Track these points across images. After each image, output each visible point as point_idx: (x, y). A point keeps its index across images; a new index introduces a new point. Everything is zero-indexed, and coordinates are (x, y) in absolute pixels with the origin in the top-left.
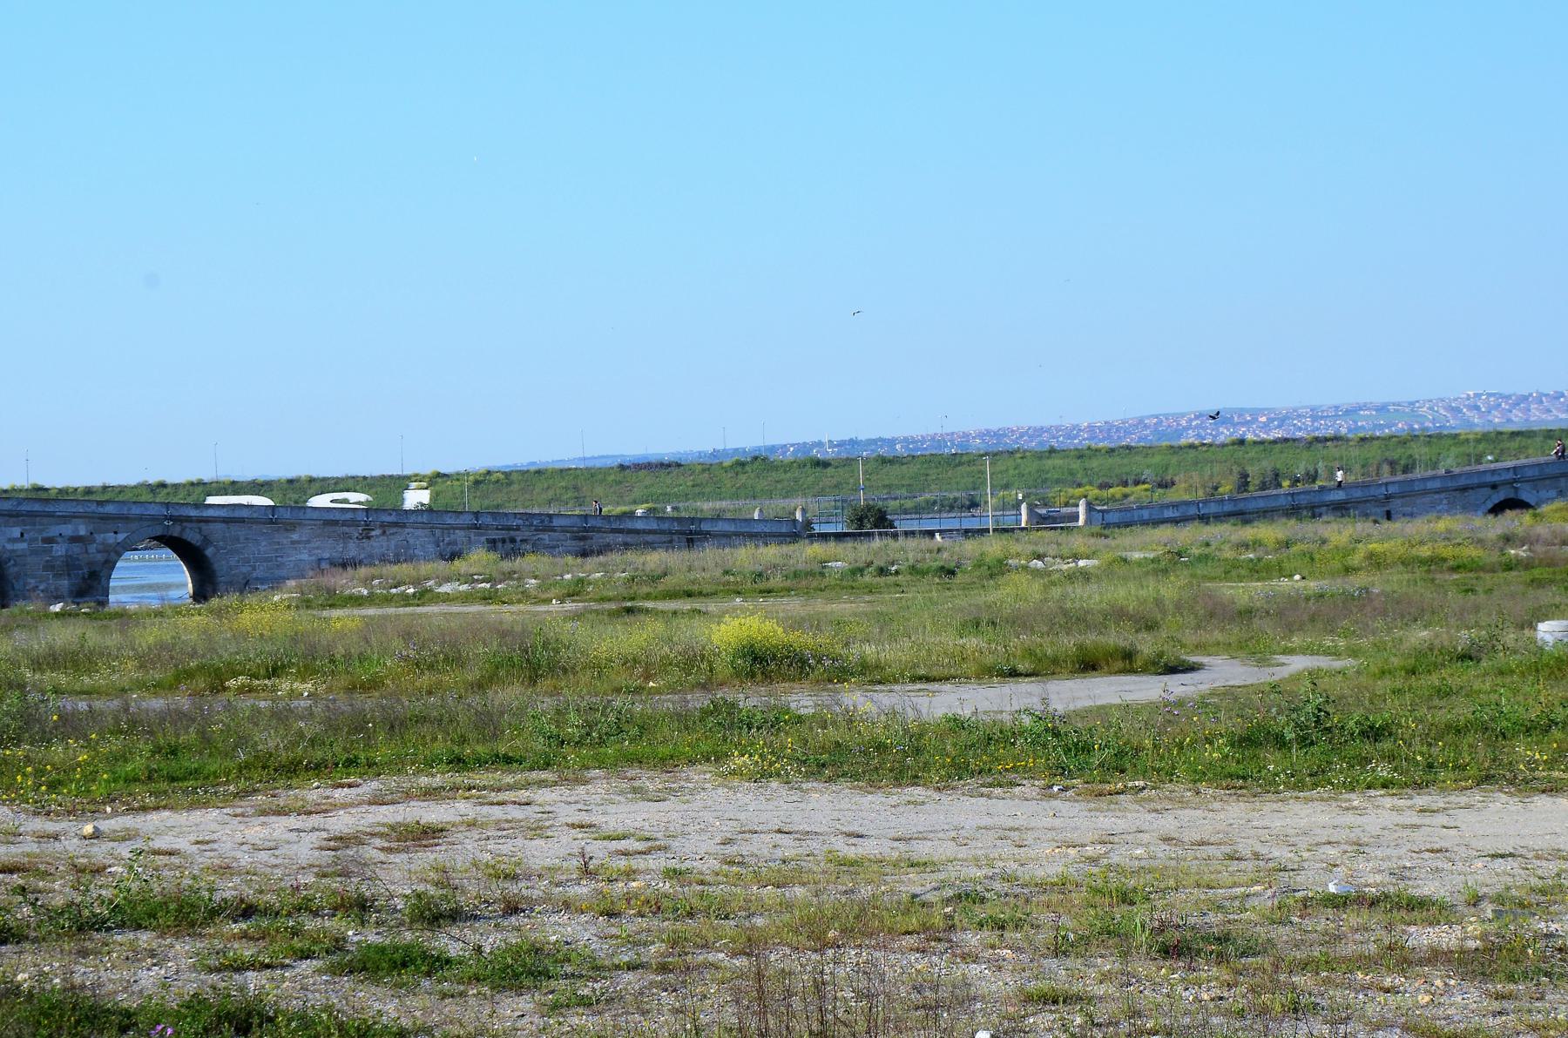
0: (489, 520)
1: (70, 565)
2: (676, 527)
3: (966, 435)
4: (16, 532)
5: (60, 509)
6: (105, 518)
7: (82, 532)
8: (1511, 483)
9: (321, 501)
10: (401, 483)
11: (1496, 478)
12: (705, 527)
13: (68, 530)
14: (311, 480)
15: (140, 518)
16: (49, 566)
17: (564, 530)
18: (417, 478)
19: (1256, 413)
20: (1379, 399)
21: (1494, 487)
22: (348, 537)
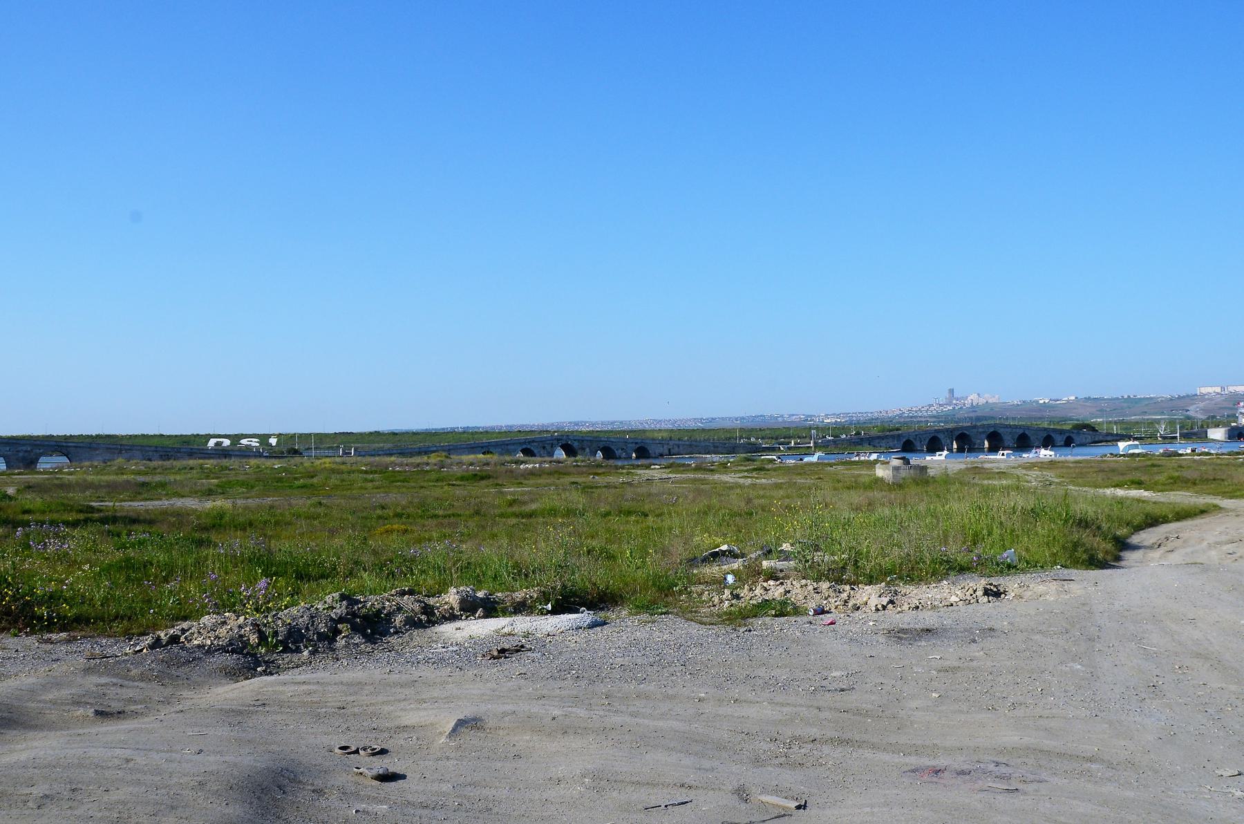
0: (160, 449)
1: (24, 459)
2: (221, 453)
3: (501, 427)
4: (8, 449)
5: (21, 442)
6: (36, 445)
7: (29, 449)
8: (487, 446)
9: (244, 442)
10: (269, 436)
11: (483, 445)
12: (230, 453)
13: (24, 448)
14: (242, 435)
15: (48, 445)
16: (17, 459)
17: (185, 452)
18: (274, 435)
19: (586, 422)
20: (621, 420)
21: (482, 447)
22: (114, 453)
